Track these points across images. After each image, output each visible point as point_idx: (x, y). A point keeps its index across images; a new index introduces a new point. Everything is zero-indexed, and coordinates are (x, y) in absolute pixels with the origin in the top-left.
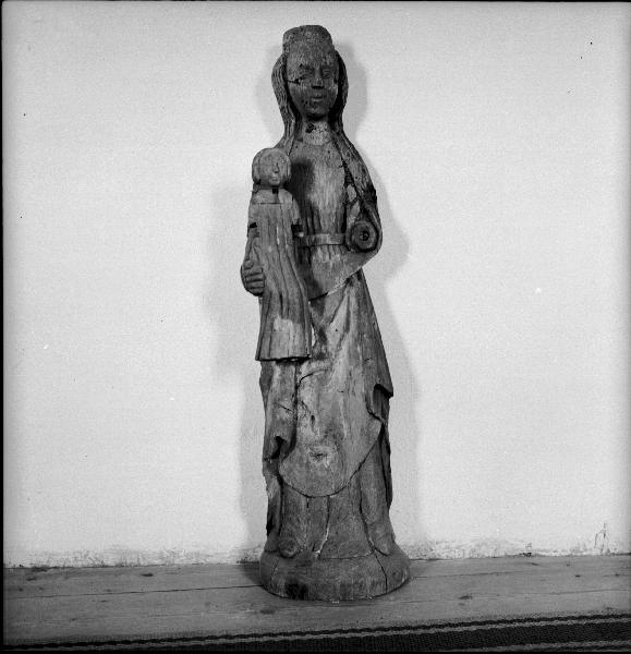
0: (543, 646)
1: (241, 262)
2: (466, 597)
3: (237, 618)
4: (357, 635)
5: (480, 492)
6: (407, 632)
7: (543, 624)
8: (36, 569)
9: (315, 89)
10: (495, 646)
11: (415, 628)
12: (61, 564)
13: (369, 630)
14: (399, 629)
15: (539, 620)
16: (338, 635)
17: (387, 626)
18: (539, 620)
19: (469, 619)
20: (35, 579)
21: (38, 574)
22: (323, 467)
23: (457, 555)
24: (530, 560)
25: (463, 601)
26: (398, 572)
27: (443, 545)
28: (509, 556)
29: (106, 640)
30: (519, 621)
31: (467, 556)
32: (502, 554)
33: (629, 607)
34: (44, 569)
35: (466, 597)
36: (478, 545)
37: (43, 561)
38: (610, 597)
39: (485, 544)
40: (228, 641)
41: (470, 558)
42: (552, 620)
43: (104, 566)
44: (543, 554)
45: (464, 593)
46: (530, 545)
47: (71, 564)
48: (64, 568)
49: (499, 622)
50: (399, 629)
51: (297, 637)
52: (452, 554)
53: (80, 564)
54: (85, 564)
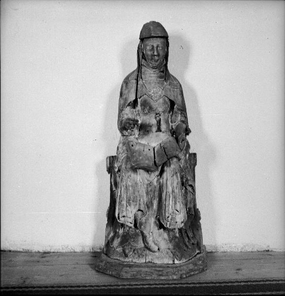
0: (274, 293)
1: (110, 141)
2: (239, 270)
3: (89, 277)
4: (189, 285)
5: (235, 222)
6: (211, 285)
7: (274, 282)
8: (45, 253)
9: (154, 48)
10: (266, 292)
11: (215, 283)
12: (56, 251)
13: (194, 283)
14: (208, 283)
15: (273, 281)
16: (155, 286)
17: (201, 282)
18: (273, 281)
19: (246, 279)
20: (44, 257)
21: (46, 255)
22: (190, 205)
23: (235, 250)
24: (269, 253)
25: (238, 271)
26: (211, 257)
27: (229, 246)
28: (259, 252)
29: (76, 285)
30: (263, 281)
31: (240, 251)
32: (255, 250)
33: (282, 276)
34: (48, 253)
35: (239, 270)
36: (245, 246)
37: (48, 249)
38: (276, 272)
39: (247, 245)
40: (130, 287)
41: (241, 252)
42: (279, 281)
43: (75, 252)
44: (274, 250)
45: (238, 267)
46: (269, 246)
47: (61, 251)
48: (57, 252)
49: (254, 281)
50: (208, 283)
51: (161, 286)
52: (232, 250)
53: (64, 251)
54: (67, 251)
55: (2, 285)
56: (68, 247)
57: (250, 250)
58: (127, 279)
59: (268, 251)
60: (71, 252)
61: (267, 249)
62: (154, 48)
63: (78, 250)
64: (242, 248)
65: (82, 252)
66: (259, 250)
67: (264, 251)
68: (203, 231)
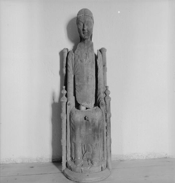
9: (80, 31)
32: (157, 157)
35: (146, 176)
44: (171, 157)
46: (167, 154)
53: (8, 163)
55: (1, 163)
56: (10, 160)
57: (153, 157)
58: (80, 132)
59: (166, 158)
60: (14, 164)
61: (165, 157)
62: (80, 31)
63: (19, 161)
64: (147, 157)
65: (22, 163)
66: (159, 157)
67: (163, 158)
68: (94, 47)
